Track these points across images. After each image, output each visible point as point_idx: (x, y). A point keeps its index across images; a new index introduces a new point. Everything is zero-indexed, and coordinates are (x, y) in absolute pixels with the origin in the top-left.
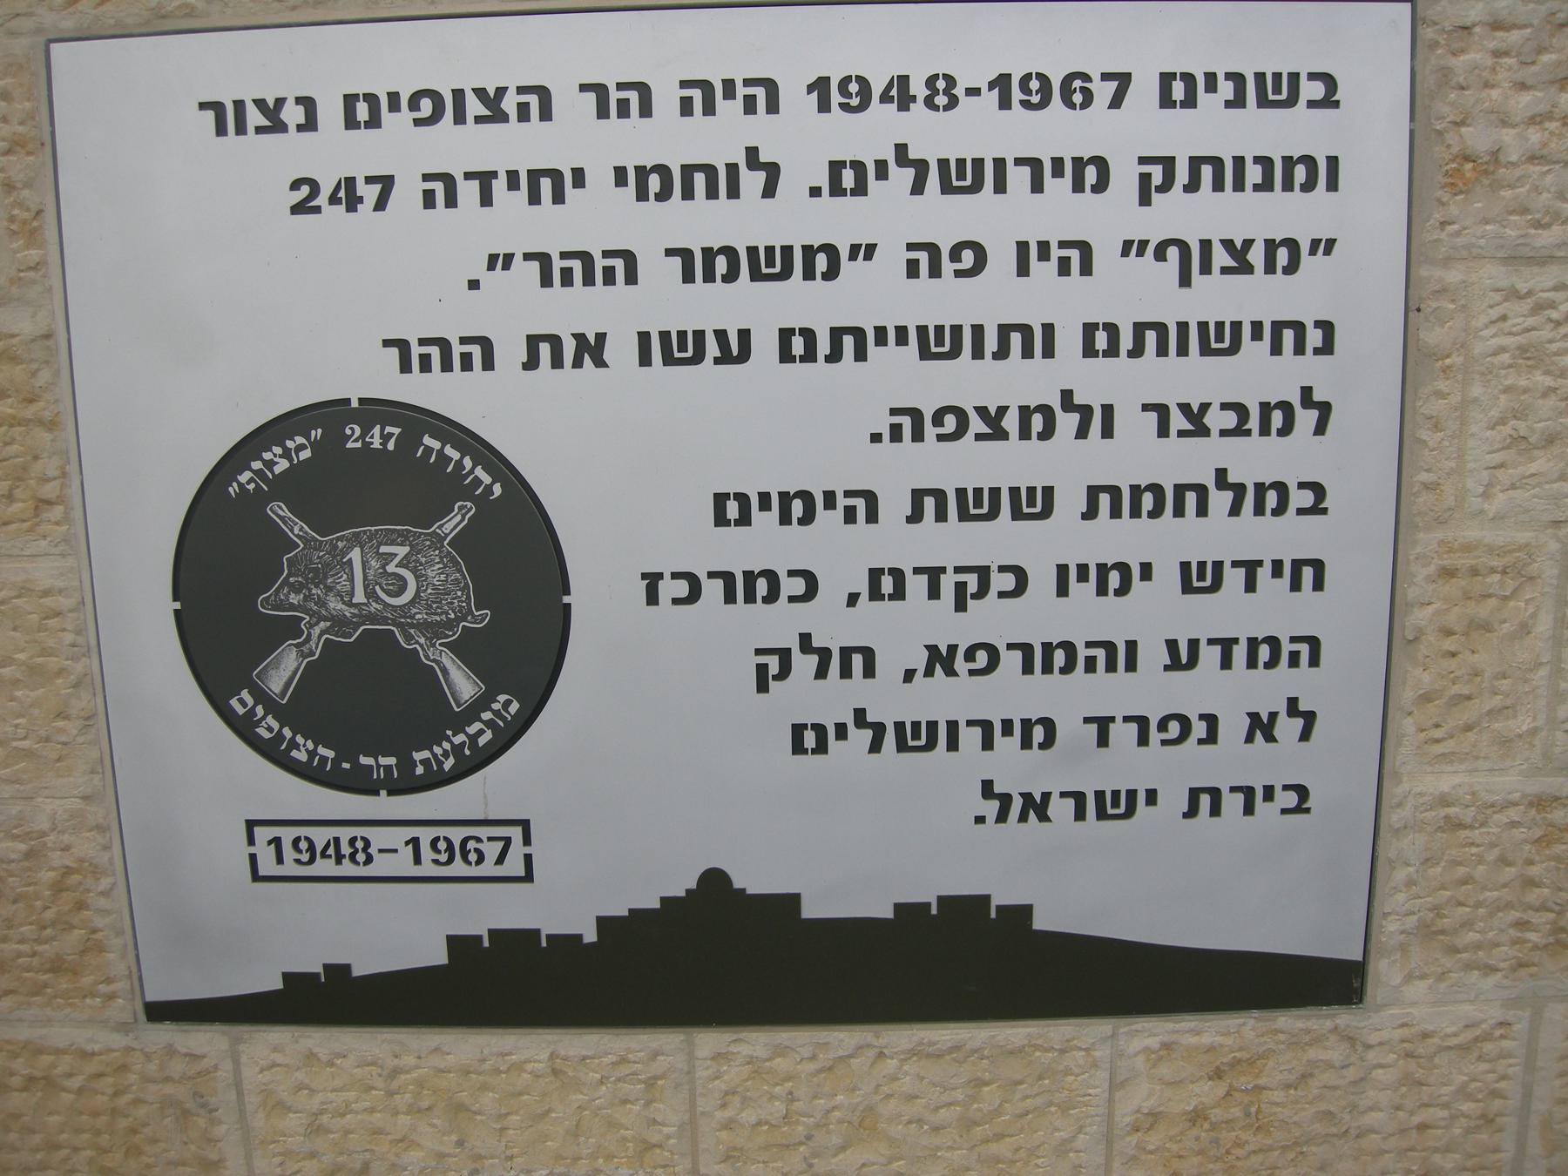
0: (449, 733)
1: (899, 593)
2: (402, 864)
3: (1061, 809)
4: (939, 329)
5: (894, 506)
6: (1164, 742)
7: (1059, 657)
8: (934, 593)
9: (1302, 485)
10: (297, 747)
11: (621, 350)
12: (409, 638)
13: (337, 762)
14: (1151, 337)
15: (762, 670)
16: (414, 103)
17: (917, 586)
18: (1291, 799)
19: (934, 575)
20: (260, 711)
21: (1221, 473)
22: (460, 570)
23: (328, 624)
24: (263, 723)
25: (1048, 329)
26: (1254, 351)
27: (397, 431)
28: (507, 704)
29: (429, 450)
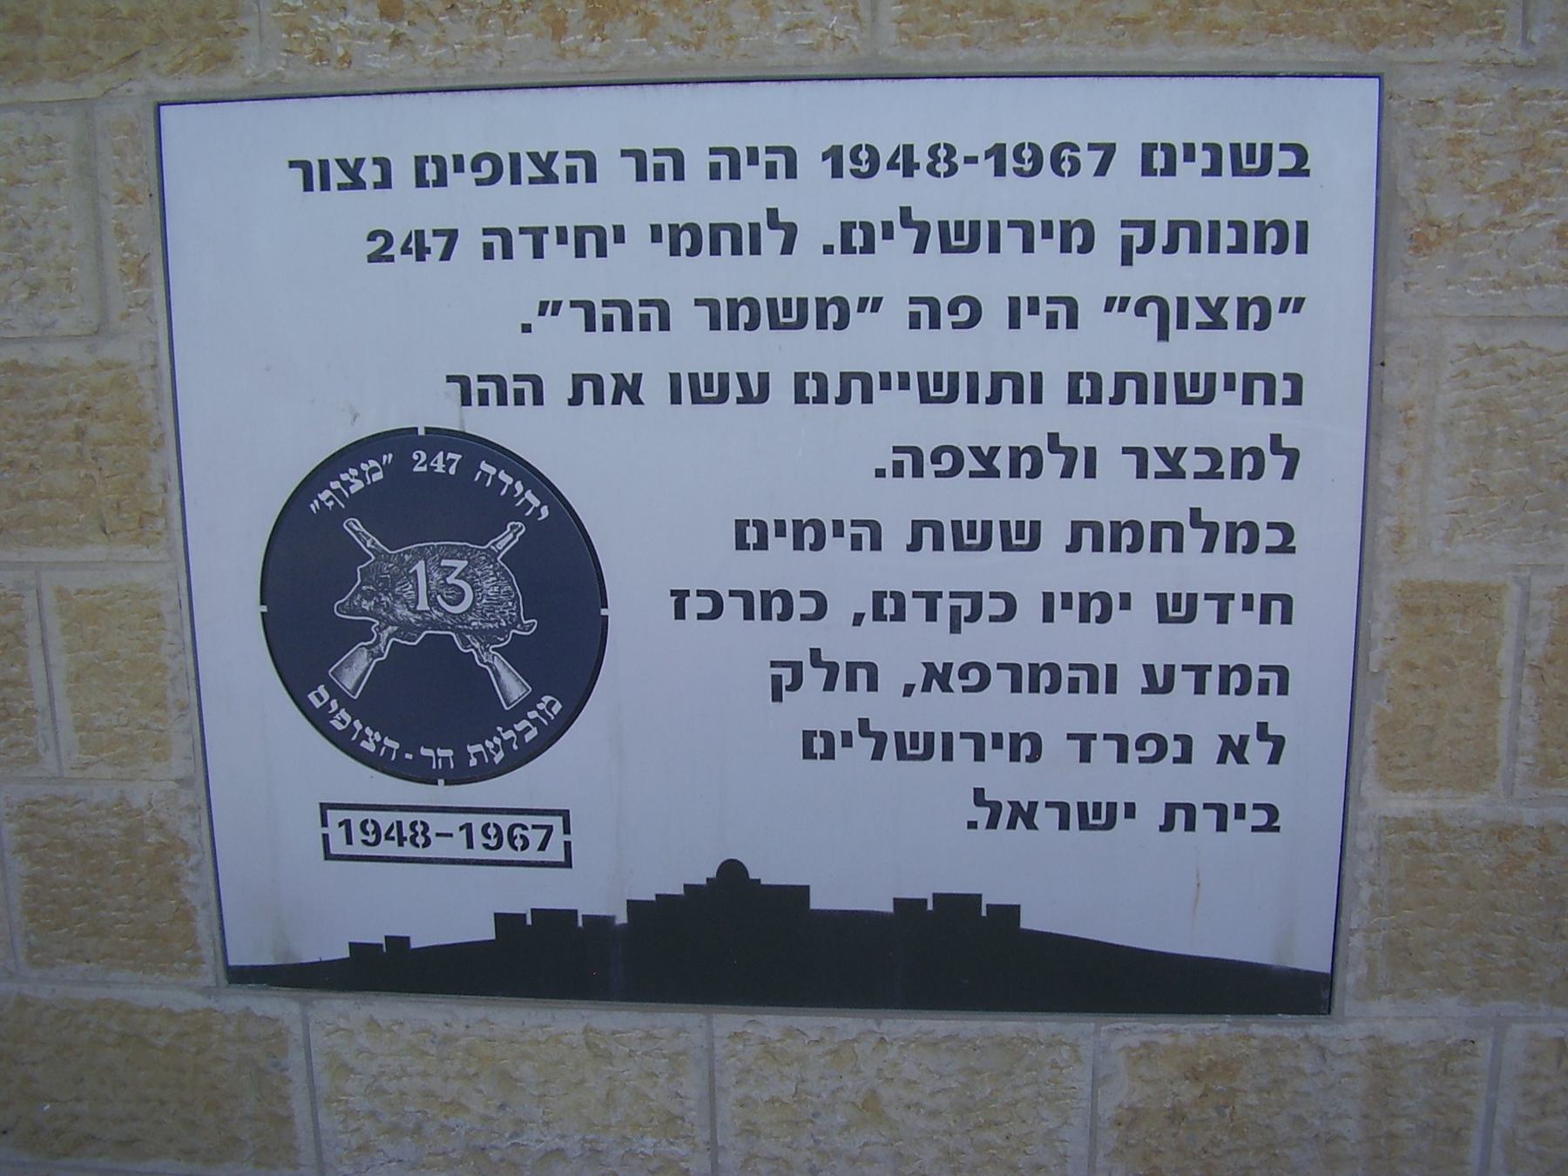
0: (500, 729)
1: (899, 615)
2: (456, 847)
3: (1047, 818)
5: (896, 535)
8: (931, 615)
9: (1271, 526)
10: (366, 738)
12: (466, 643)
13: (400, 752)
15: (776, 680)
17: (916, 608)
19: (932, 599)
20: (334, 705)
23: (395, 628)
24: (337, 716)
26: (1228, 401)
27: (458, 457)
28: (551, 704)
29: (485, 475)
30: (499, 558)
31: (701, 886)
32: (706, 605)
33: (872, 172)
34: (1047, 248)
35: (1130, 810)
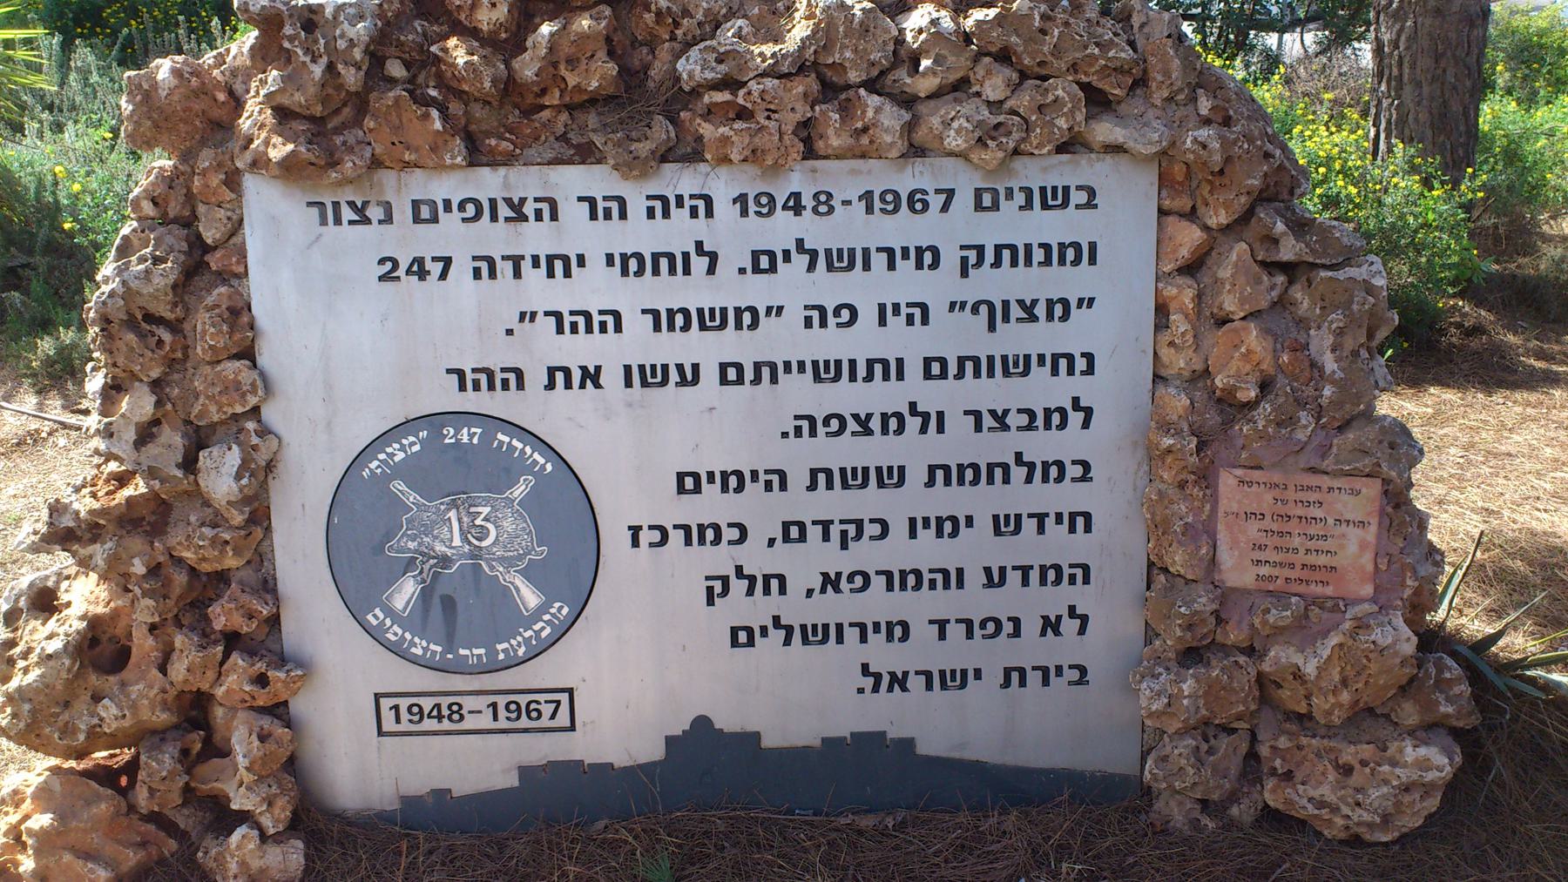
0: (521, 630)
1: (802, 538)
2: (486, 721)
4: (827, 363)
5: (798, 478)
7: (911, 580)
8: (826, 537)
9: (1074, 462)
10: (415, 645)
12: (492, 568)
14: (969, 366)
15: (710, 590)
17: (814, 532)
18: (1075, 675)
19: (826, 525)
20: (388, 622)
21: (1019, 456)
22: (526, 522)
23: (436, 561)
24: (391, 631)
25: (900, 362)
26: (1040, 374)
27: (479, 431)
28: (560, 608)
29: (501, 443)
30: (515, 504)
31: (678, 736)
32: (656, 536)
33: (771, 213)
34: (905, 267)
35: (978, 674)
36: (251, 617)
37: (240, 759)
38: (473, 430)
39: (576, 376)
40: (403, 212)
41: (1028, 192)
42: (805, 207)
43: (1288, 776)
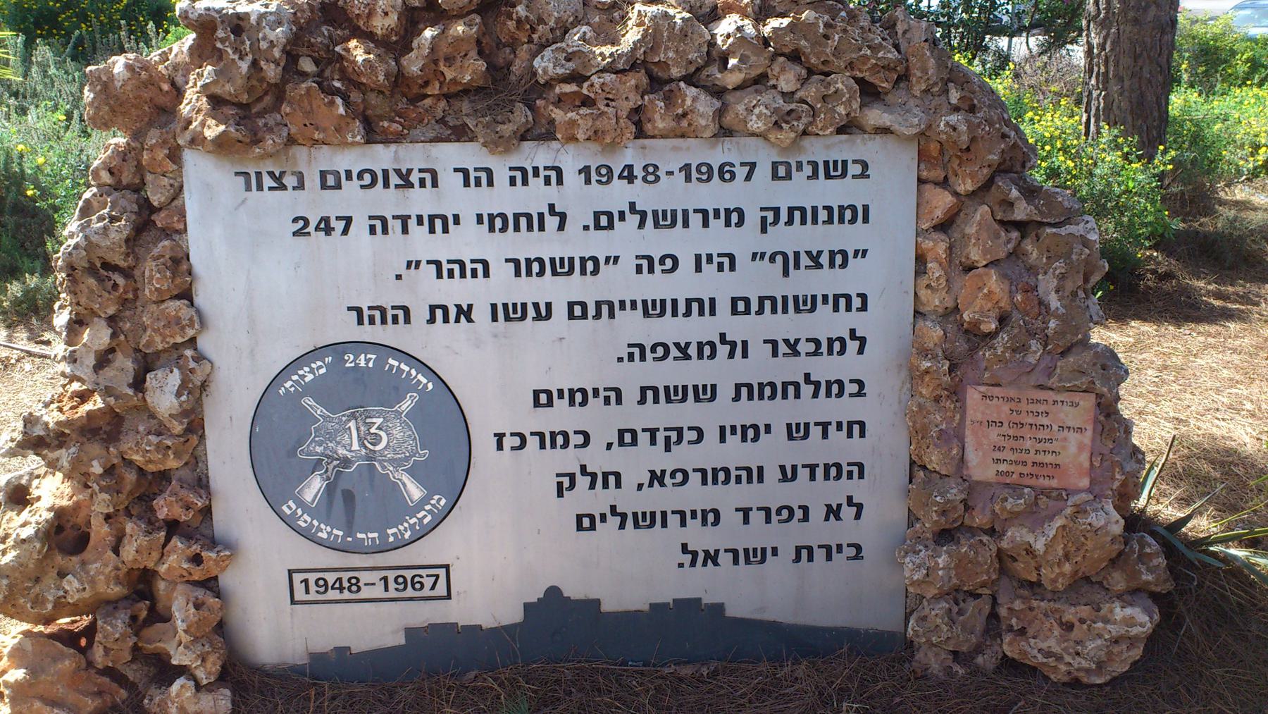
0: (407, 518)
1: (634, 442)
2: (378, 592)
3: (726, 559)
5: (630, 395)
6: (780, 521)
7: (721, 476)
8: (653, 441)
11: (481, 314)
12: (384, 468)
13: (344, 537)
14: (768, 304)
15: (560, 485)
16: (360, 176)
17: (644, 438)
19: (653, 432)
20: (299, 512)
21: (807, 376)
22: (412, 430)
23: (338, 462)
25: (712, 301)
26: (824, 310)
27: (374, 357)
28: (439, 500)
29: (392, 366)
32: (517, 441)
33: (608, 181)
34: (717, 224)
35: (775, 551)
36: (188, 508)
37: (179, 623)
38: (369, 356)
39: (453, 312)
40: (312, 180)
41: (814, 165)
42: (636, 177)
43: (1022, 632)
